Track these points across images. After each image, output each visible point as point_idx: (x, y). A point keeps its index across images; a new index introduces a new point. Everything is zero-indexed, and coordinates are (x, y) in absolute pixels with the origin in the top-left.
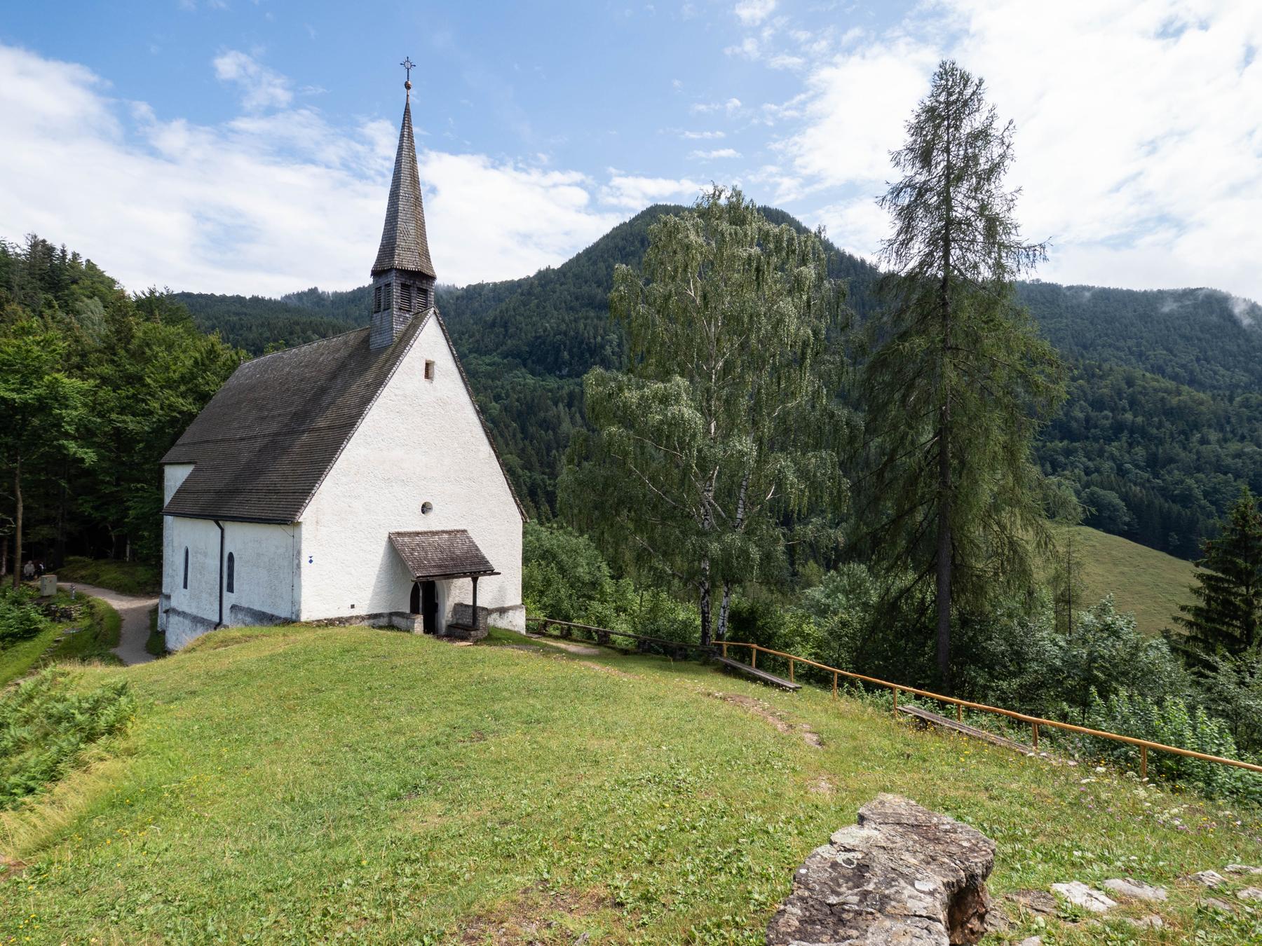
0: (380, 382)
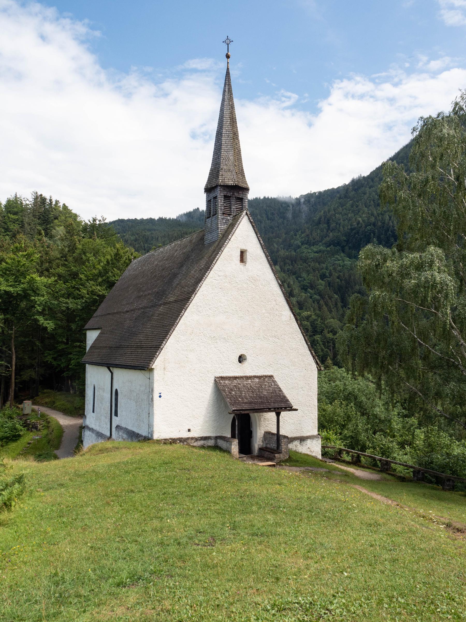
0: (208, 267)
